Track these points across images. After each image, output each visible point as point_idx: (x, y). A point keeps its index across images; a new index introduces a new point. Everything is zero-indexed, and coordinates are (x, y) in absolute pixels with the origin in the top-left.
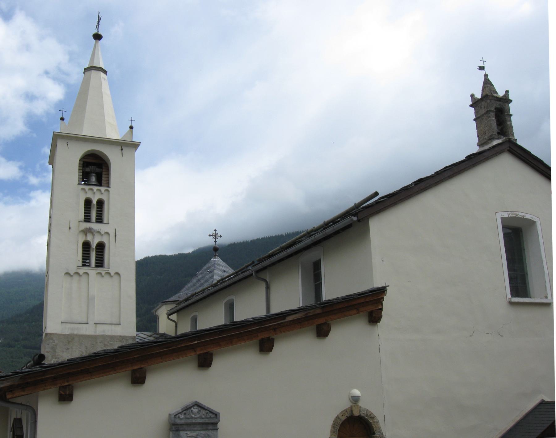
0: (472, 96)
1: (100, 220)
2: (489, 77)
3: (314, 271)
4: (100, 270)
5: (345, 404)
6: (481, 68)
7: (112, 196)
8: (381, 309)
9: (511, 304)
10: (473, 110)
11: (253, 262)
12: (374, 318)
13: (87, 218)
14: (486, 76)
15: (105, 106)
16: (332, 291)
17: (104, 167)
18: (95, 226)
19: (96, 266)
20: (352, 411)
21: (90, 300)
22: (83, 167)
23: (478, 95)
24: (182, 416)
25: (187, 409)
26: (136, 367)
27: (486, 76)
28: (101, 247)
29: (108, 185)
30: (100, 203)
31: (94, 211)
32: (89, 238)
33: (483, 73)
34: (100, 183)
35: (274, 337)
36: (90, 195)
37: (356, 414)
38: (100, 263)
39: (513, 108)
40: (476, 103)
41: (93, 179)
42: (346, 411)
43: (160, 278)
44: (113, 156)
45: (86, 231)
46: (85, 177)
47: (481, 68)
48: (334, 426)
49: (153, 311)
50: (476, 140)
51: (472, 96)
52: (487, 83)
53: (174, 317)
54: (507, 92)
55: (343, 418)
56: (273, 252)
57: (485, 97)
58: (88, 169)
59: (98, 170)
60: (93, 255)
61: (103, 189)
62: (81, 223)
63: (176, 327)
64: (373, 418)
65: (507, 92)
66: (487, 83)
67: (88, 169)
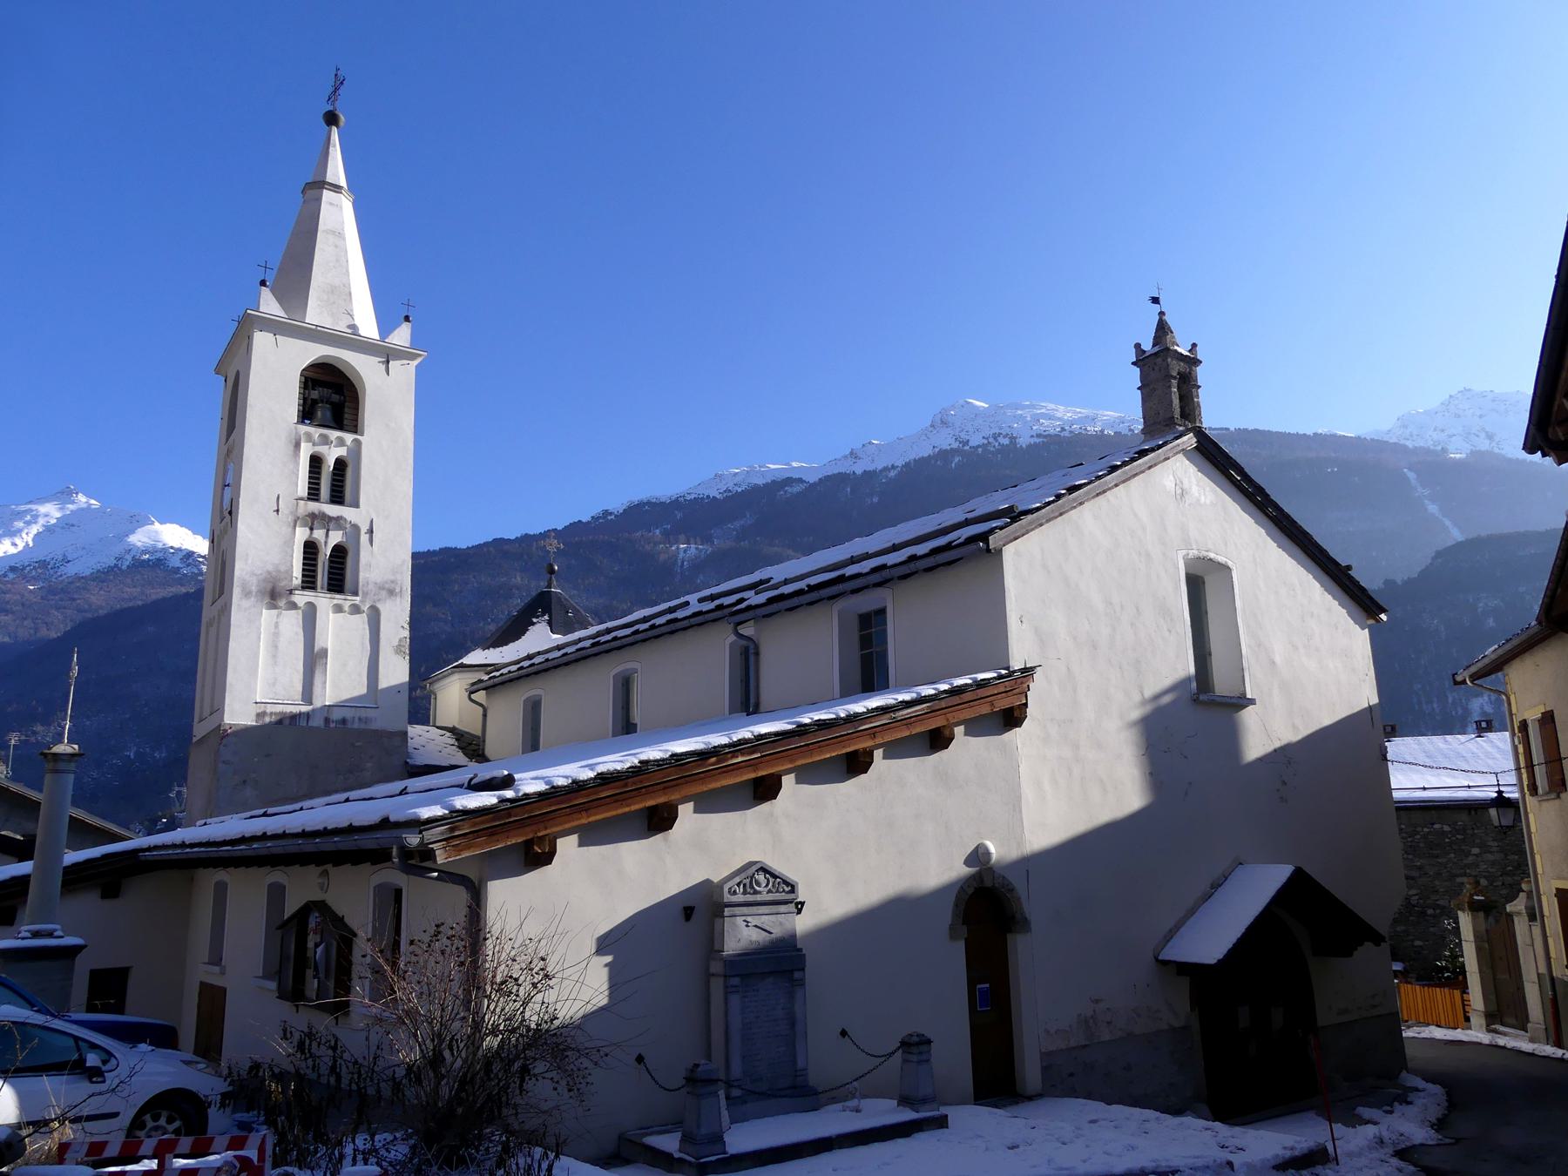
0: (1138, 346)
2: (1166, 318)
4: (338, 598)
6: (1155, 300)
13: (314, 494)
14: (1162, 313)
15: (912, 523)
18: (333, 510)
19: (330, 590)
21: (314, 659)
27: (1162, 313)
32: (319, 534)
34: (339, 425)
37: (988, 883)
39: (1201, 373)
45: (314, 520)
47: (1155, 300)
48: (956, 905)
51: (1138, 346)
52: (1162, 329)
53: (480, 696)
55: (970, 891)
59: (335, 398)
63: (485, 715)
64: (1012, 890)
66: (1162, 329)
67: (315, 394)
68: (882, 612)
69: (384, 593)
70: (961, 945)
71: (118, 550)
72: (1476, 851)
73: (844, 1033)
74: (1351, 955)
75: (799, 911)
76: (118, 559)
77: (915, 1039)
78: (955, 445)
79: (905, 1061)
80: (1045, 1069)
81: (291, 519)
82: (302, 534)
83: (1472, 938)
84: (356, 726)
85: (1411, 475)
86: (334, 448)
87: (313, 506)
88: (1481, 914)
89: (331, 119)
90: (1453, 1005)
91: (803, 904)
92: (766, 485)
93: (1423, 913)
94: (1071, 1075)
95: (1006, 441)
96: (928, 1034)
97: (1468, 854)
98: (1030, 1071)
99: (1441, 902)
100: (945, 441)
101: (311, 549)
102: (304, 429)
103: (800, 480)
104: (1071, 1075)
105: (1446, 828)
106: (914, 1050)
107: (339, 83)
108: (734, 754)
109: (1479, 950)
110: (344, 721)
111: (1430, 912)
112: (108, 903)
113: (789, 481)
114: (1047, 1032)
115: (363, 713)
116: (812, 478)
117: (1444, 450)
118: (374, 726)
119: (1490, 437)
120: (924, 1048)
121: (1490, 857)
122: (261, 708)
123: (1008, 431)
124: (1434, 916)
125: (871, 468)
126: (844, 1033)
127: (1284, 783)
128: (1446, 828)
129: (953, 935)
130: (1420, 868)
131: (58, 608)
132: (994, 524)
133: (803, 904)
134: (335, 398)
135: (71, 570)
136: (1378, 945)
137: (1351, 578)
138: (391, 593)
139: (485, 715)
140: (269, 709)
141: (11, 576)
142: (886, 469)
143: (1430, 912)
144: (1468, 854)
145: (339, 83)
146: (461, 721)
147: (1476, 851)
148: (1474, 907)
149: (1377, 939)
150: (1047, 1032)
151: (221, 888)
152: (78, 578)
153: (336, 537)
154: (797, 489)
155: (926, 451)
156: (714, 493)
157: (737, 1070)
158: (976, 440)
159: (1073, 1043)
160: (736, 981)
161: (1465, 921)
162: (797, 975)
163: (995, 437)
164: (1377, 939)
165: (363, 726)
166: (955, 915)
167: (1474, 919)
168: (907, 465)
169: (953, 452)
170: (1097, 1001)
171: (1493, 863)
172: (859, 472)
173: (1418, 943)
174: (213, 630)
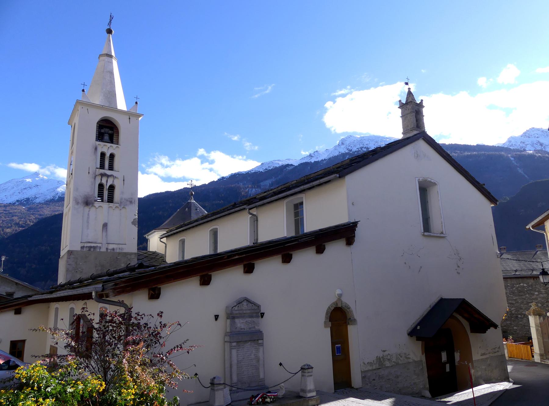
1: (111, 168)
3: (295, 210)
4: (111, 204)
5: (334, 300)
7: (118, 150)
8: (354, 236)
9: (424, 235)
10: (400, 110)
11: (235, 204)
12: (350, 242)
13: (102, 166)
14: (409, 89)
16: (313, 223)
17: (115, 130)
18: (109, 172)
20: (337, 304)
22: (99, 128)
23: (404, 101)
24: (236, 308)
25: (239, 303)
26: (204, 273)
27: (409, 89)
28: (112, 188)
29: (117, 143)
30: (112, 156)
31: (107, 162)
32: (104, 181)
33: (407, 87)
34: (111, 141)
35: (291, 253)
36: (105, 150)
37: (340, 306)
38: (111, 200)
39: (425, 111)
40: (402, 106)
41: (106, 137)
42: (334, 303)
43: (160, 211)
44: (122, 123)
46: (100, 137)
48: (327, 314)
49: (146, 236)
50: (402, 131)
53: (164, 240)
54: (422, 100)
55: (332, 308)
56: (263, 197)
57: (407, 103)
58: (103, 131)
59: (110, 132)
60: (106, 193)
61: (114, 146)
62: (97, 170)
63: (166, 247)
64: (349, 308)
65: (422, 100)
66: (410, 93)
67: (103, 131)
68: (302, 204)
69: (128, 203)
70: (328, 330)
71: (53, 194)
72: (536, 293)
73: (281, 364)
74: (485, 332)
75: (262, 317)
76: (53, 197)
77: (306, 367)
78: (347, 151)
79: (303, 376)
80: (363, 378)
81: (94, 176)
82: (98, 182)
83: (534, 326)
84: (118, 251)
85: (512, 159)
86: (107, 148)
87: (102, 171)
88: (538, 317)
89: (109, 31)
90: (528, 351)
91: (264, 314)
92: (280, 167)
93: (517, 317)
94: (374, 380)
95: (365, 150)
96: (312, 365)
97: (534, 295)
98: (356, 380)
99: (523, 313)
100: (343, 150)
101: (101, 186)
102: (98, 143)
103: (292, 165)
104: (374, 380)
105: (525, 285)
106: (306, 371)
107: (111, 18)
108: (235, 255)
109: (537, 330)
110: (113, 249)
111: (519, 316)
112: (18, 316)
113: (288, 165)
114: (364, 364)
115: (121, 246)
116: (296, 164)
117: (525, 150)
118: (125, 251)
119: (541, 145)
120: (310, 370)
121: (541, 295)
122: (83, 245)
123: (366, 146)
124: (521, 318)
125: (317, 160)
126: (281, 364)
127: (458, 267)
128: (525, 285)
129: (326, 326)
130: (515, 300)
131: (33, 214)
132: (438, 235)
133: (264, 314)
134: (110, 132)
135: (38, 201)
136: (496, 328)
137: (483, 188)
138: (131, 202)
139: (166, 247)
140: (86, 245)
141: (17, 203)
142: (322, 160)
143: (519, 316)
144: (534, 295)
145: (111, 18)
146: (158, 249)
147: (536, 293)
148: (535, 314)
149: (495, 326)
150: (364, 364)
151: (57, 309)
152: (40, 203)
153: (110, 182)
154: (291, 168)
155: (336, 154)
156: (261, 170)
157: (235, 379)
158: (355, 149)
159: (374, 368)
160: (234, 344)
161: (532, 320)
162: (260, 341)
163: (361, 148)
164: (495, 326)
165: (120, 251)
166: (326, 318)
167: (535, 318)
168: (330, 158)
169: (347, 154)
170: (384, 351)
171: (543, 298)
172: (313, 161)
173: (515, 328)
174: (67, 217)
